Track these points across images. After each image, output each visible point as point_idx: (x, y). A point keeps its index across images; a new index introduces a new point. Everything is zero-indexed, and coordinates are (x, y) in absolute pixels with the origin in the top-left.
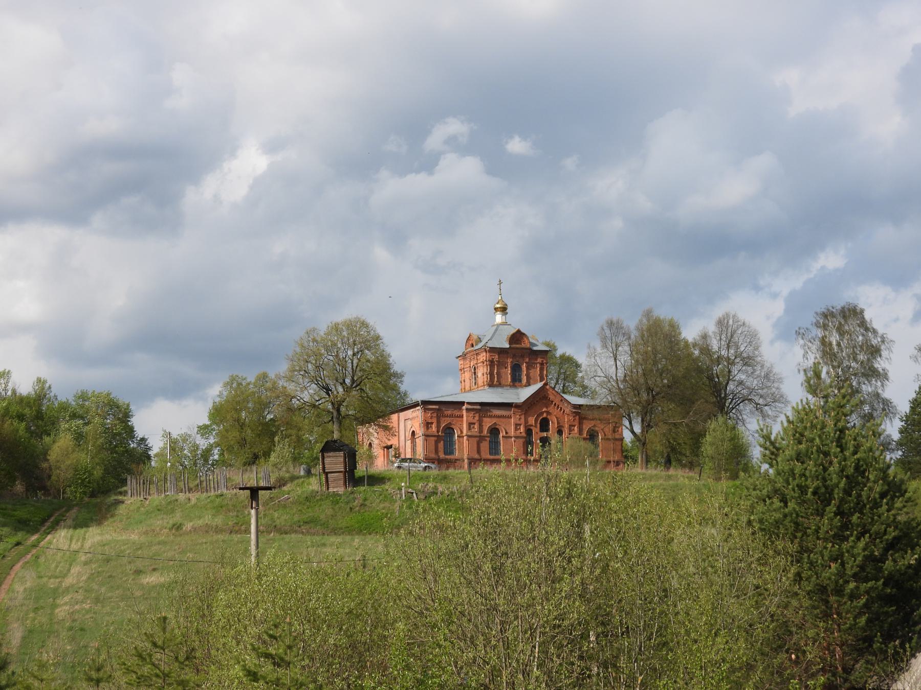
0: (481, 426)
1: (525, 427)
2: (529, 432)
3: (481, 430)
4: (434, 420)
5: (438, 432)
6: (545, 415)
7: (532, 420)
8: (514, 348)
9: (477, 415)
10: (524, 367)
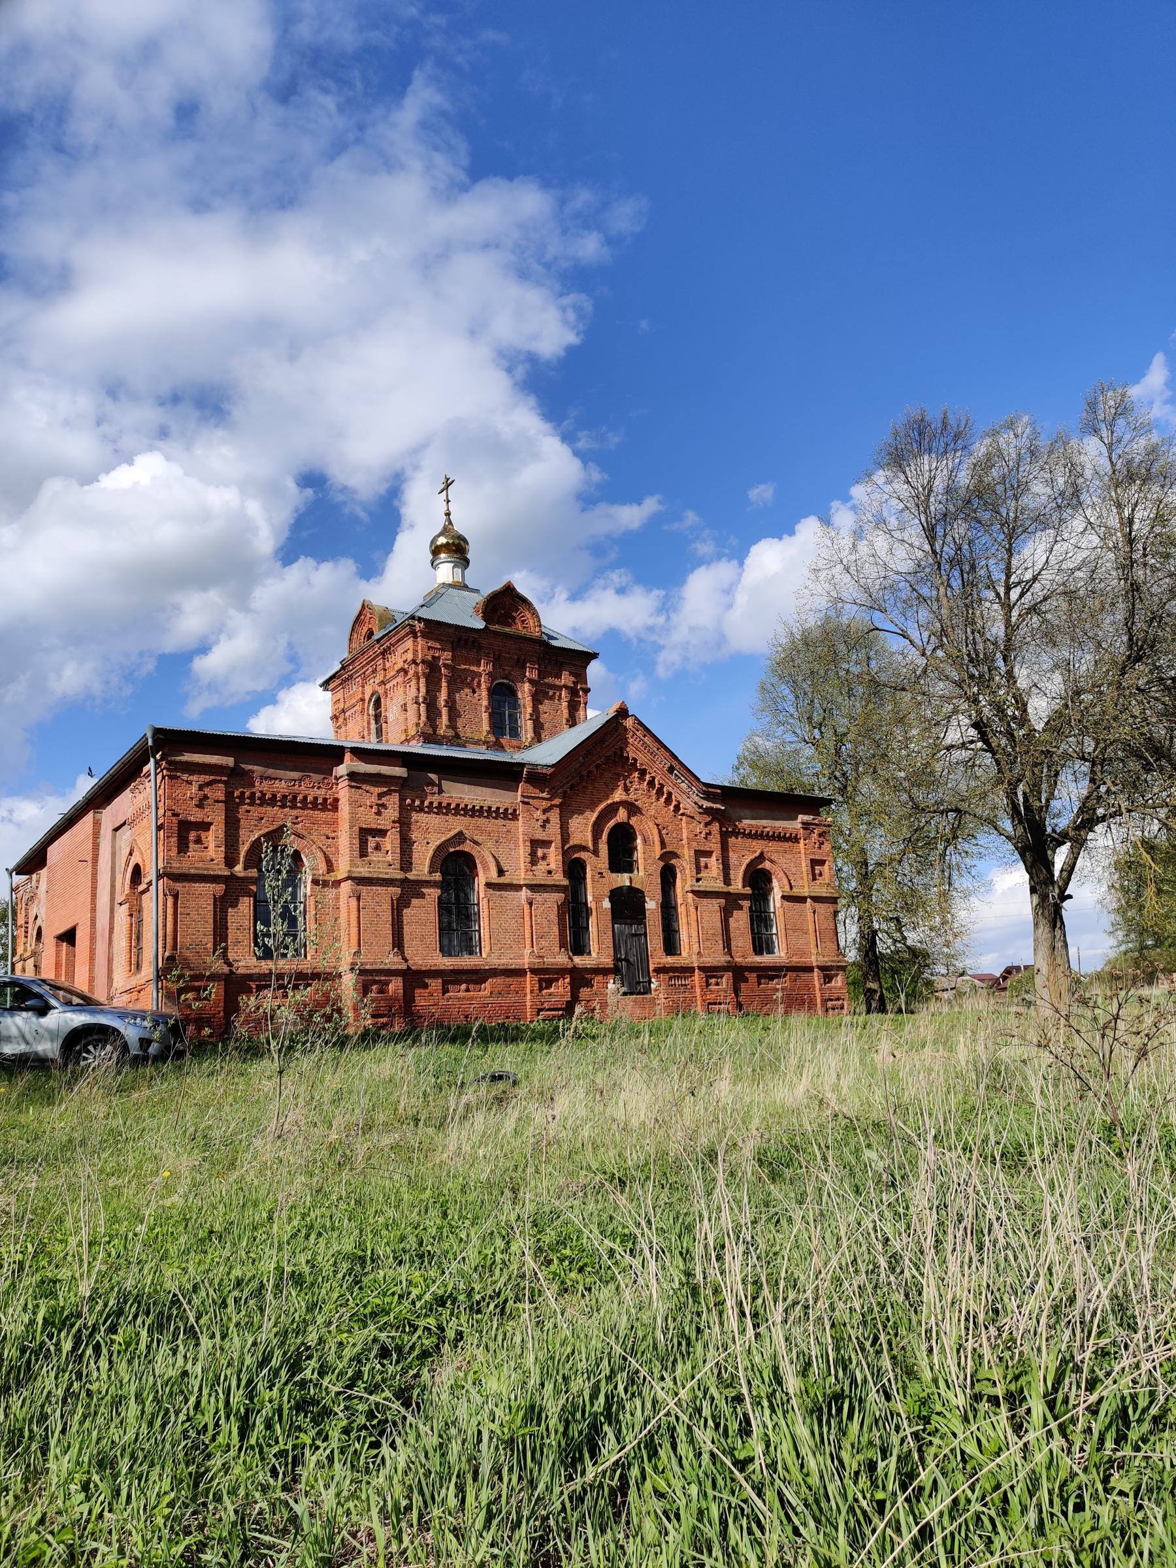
0: (406, 844)
1: (565, 853)
2: (575, 870)
3: (406, 863)
4: (216, 816)
5: (230, 861)
6: (622, 815)
7: (581, 828)
8: (496, 633)
9: (393, 801)
10: (525, 691)
